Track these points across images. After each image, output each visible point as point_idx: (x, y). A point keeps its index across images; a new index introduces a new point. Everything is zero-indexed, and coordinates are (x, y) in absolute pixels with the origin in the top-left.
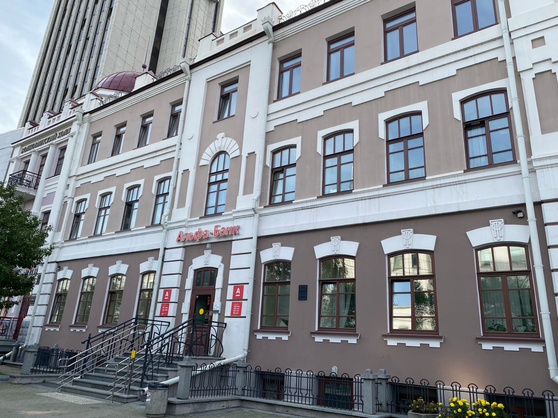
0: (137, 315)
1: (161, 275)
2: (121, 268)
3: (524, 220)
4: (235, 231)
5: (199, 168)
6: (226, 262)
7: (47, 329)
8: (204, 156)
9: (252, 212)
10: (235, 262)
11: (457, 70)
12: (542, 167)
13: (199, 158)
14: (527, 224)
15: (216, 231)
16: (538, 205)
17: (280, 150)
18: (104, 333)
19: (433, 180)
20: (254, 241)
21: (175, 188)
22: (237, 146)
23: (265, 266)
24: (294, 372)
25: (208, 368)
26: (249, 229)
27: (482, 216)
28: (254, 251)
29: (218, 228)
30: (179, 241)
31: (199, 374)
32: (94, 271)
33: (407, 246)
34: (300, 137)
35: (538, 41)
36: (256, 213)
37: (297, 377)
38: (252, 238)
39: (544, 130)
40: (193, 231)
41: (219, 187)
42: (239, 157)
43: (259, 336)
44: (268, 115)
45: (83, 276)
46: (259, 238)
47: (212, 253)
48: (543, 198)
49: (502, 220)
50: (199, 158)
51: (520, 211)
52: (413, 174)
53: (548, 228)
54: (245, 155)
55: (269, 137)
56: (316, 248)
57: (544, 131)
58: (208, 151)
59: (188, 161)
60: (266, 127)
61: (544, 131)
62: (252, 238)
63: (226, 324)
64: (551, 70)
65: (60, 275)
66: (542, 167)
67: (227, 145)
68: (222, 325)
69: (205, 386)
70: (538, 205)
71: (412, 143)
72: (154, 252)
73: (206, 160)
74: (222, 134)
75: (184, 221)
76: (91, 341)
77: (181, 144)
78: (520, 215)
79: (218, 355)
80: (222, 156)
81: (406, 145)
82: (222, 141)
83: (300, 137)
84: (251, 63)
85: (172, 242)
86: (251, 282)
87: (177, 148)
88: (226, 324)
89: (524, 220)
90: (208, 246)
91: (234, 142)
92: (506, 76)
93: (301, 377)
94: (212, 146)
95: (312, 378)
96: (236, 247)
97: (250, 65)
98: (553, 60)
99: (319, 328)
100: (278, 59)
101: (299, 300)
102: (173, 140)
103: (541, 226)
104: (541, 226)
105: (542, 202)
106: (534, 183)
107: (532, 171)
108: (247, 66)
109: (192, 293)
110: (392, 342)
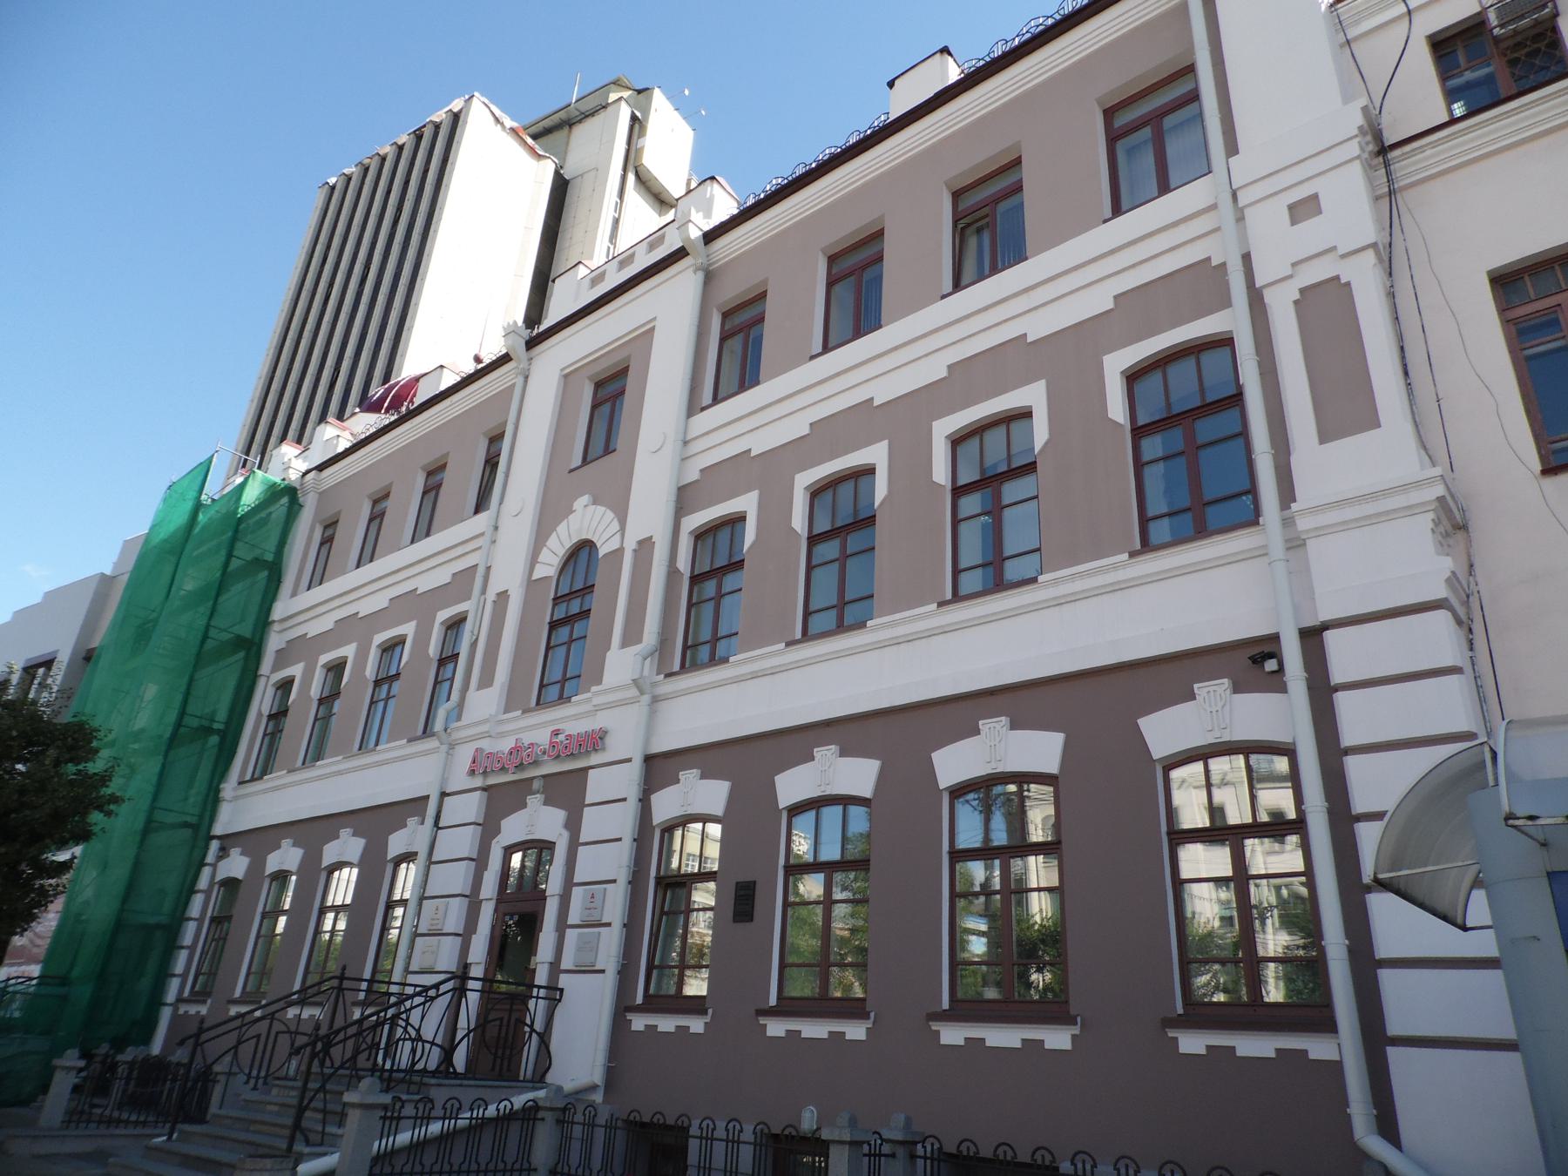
0: (375, 971)
1: (430, 862)
2: (287, 857)
3: (1276, 682)
4: (595, 741)
5: (532, 585)
6: (573, 825)
7: (181, 1011)
8: (545, 555)
9: (634, 692)
10: (594, 823)
11: (1116, 297)
12: (1320, 531)
13: (533, 561)
14: (1282, 688)
15: (553, 745)
16: (1312, 637)
17: (978, 430)
18: (242, 1015)
19: (1056, 581)
20: (634, 771)
21: (474, 644)
22: (616, 526)
23: (951, 793)
24: (721, 1125)
25: (491, 1111)
26: (627, 738)
27: (1171, 675)
28: (632, 792)
29: (561, 737)
30: (472, 772)
31: (462, 1131)
32: (857, 775)
33: (993, 765)
34: (886, 442)
35: (1305, 209)
36: (642, 693)
37: (727, 1141)
38: (629, 760)
39: (1327, 433)
40: (506, 745)
41: (719, 586)
42: (619, 552)
43: (639, 1023)
44: (686, 443)
45: (325, 863)
46: (649, 759)
47: (545, 804)
48: (1325, 615)
49: (1225, 681)
50: (533, 561)
51: (1271, 656)
52: (1012, 570)
53: (1341, 698)
54: (630, 545)
55: (685, 500)
56: (939, 757)
57: (1325, 436)
58: (552, 542)
59: (508, 575)
60: (680, 472)
61: (1325, 436)
62: (629, 760)
63: (562, 990)
64: (1337, 278)
65: (666, 805)
66: (1320, 531)
67: (594, 524)
68: (555, 994)
69: (483, 1161)
70: (1312, 637)
71: (1207, 428)
72: (416, 805)
73: (548, 566)
74: (585, 499)
75: (485, 721)
76: (204, 1037)
77: (496, 528)
78: (1271, 665)
79: (539, 1079)
80: (584, 554)
81: (1190, 437)
82: (588, 520)
83: (886, 442)
84: (657, 323)
85: (459, 780)
86: (623, 877)
87: (487, 538)
88: (562, 990)
89: (1276, 682)
90: (536, 785)
91: (610, 515)
92: (1225, 302)
93: (739, 1142)
94: (562, 528)
95: (932, 1159)
96: (599, 785)
97: (653, 329)
98: (1341, 251)
99: (779, 998)
100: (823, 251)
101: (735, 921)
102: (483, 520)
103: (1322, 693)
104: (1322, 693)
105: (1326, 626)
106: (1301, 575)
107: (1296, 544)
108: (645, 336)
109: (496, 910)
110: (1192, 1043)
